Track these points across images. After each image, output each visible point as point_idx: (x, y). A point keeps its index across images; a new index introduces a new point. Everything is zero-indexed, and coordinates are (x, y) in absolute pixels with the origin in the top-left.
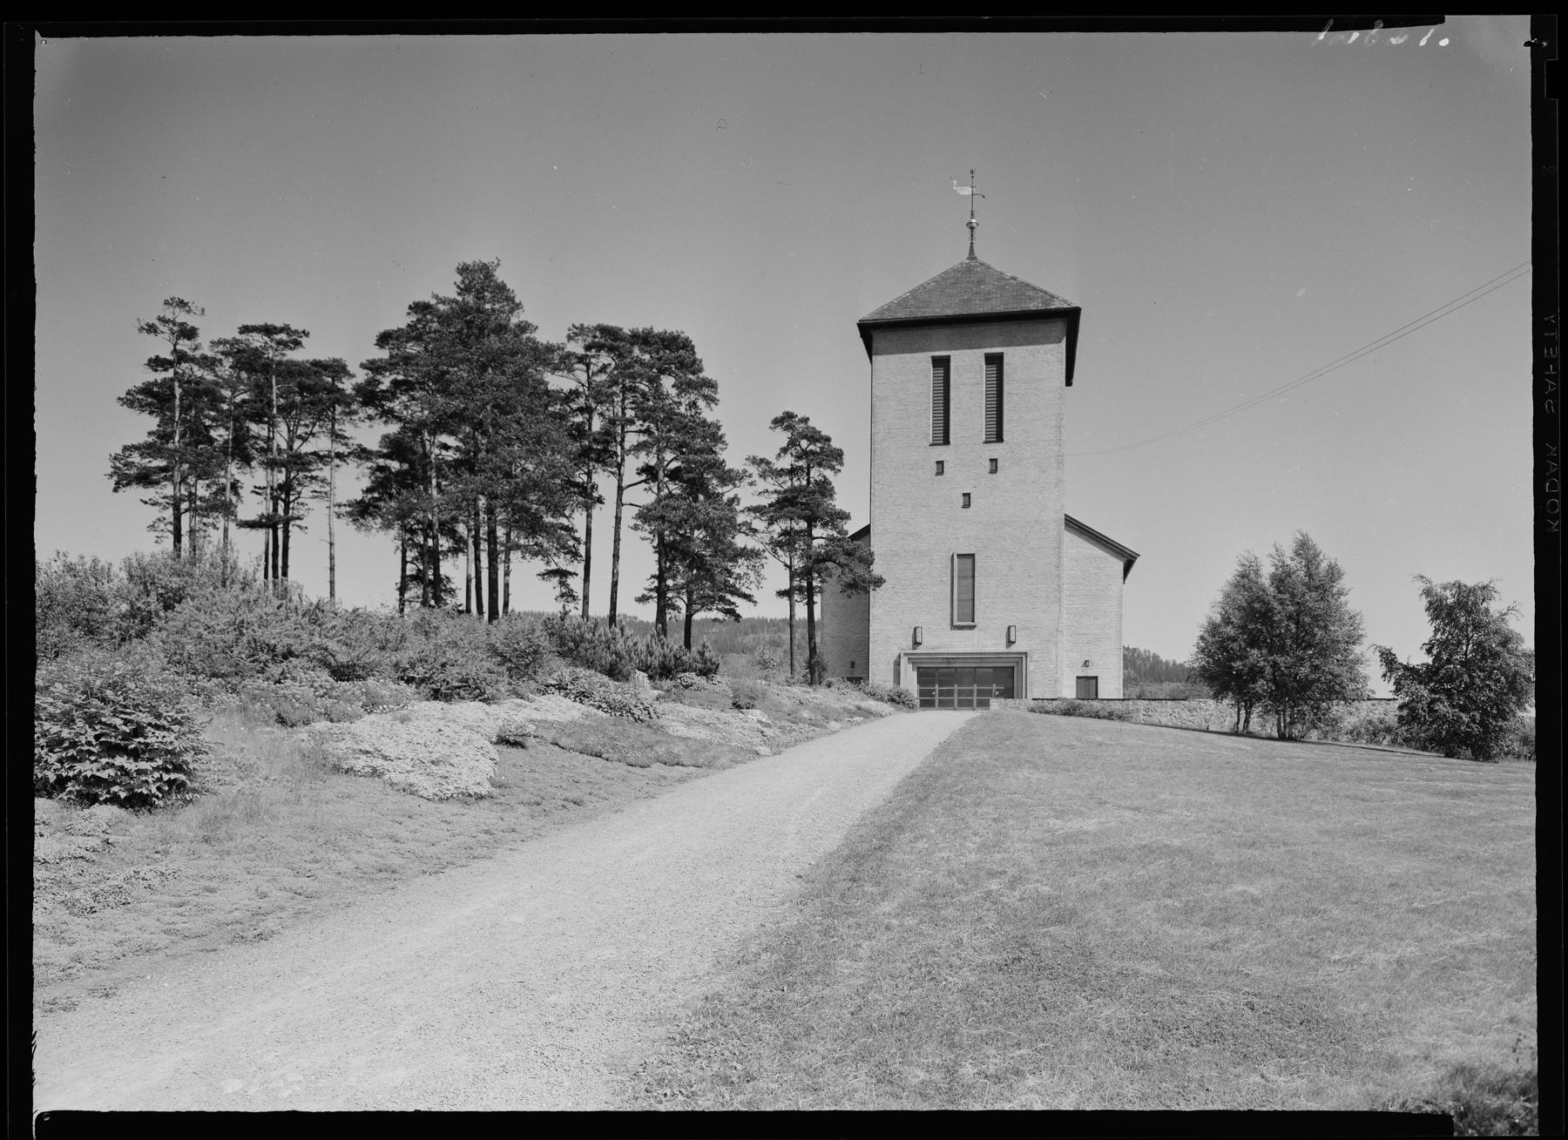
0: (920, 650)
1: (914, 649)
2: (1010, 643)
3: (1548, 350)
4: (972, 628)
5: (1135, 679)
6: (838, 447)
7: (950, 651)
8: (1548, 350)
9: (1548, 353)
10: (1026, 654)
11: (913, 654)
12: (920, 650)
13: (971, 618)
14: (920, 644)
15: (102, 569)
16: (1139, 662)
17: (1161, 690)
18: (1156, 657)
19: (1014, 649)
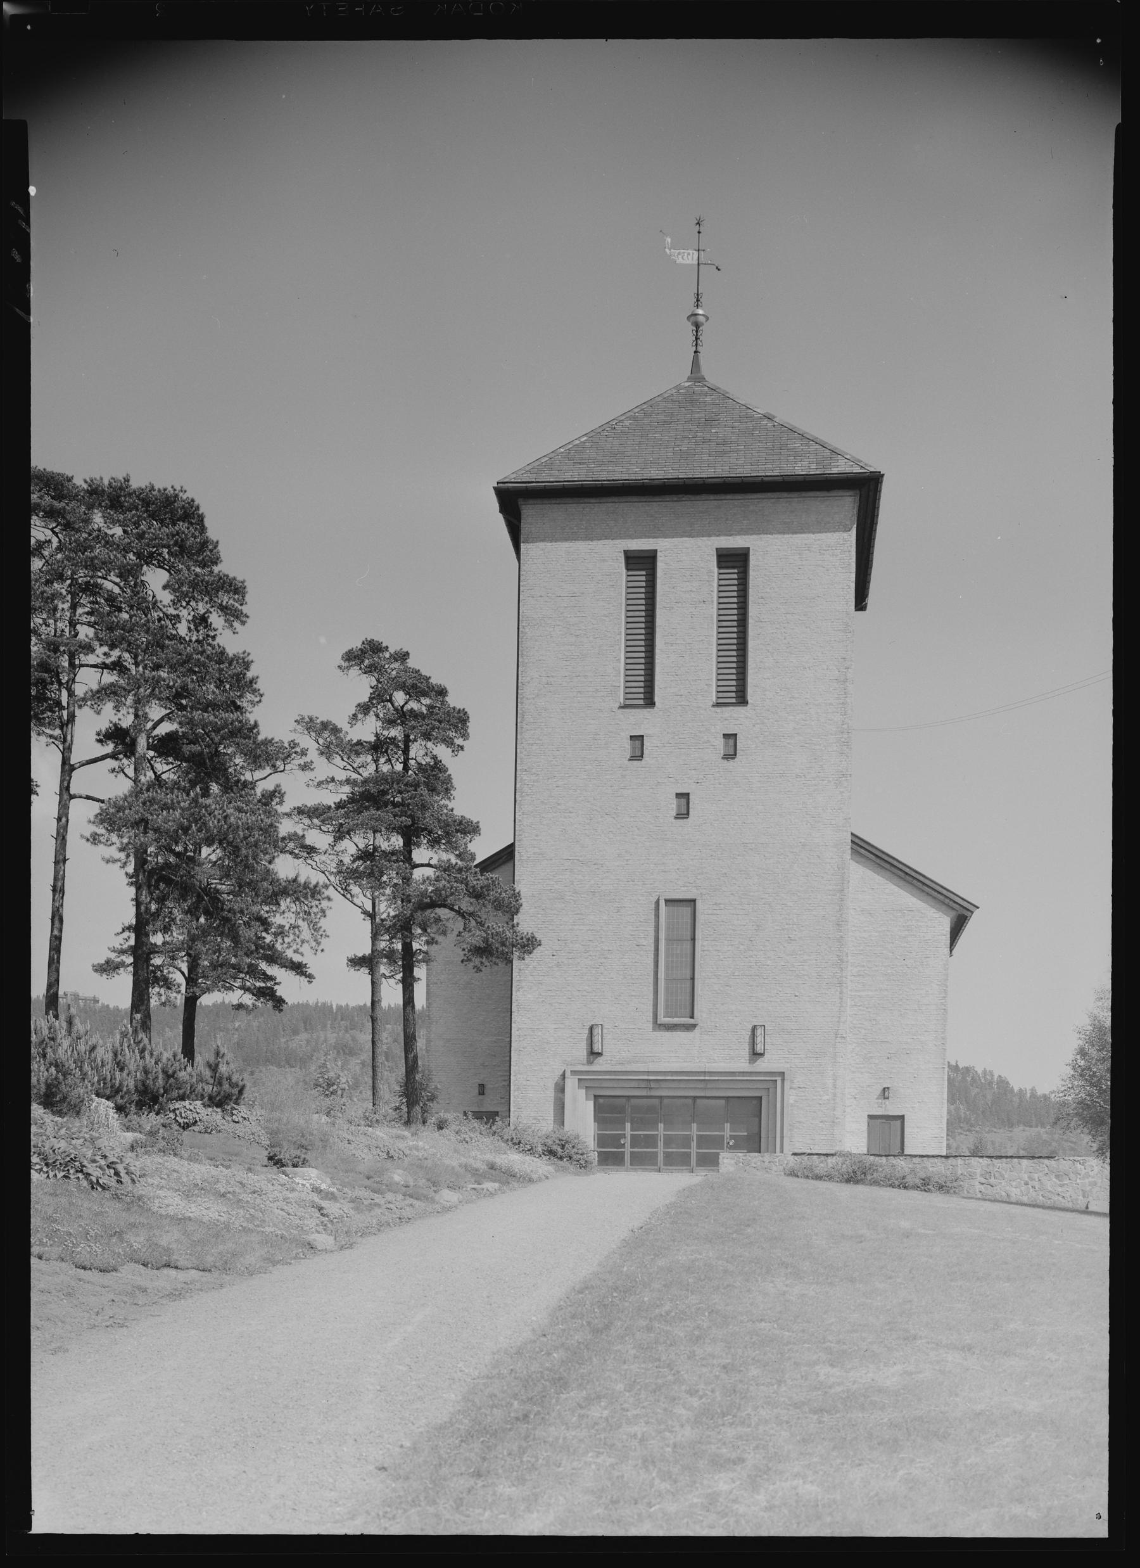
0: (600, 1065)
1: (590, 1063)
2: (755, 1055)
7: (652, 1067)
10: (782, 1074)
12: (600, 1065)
16: (974, 1091)
17: (1010, 1139)
19: (762, 1065)
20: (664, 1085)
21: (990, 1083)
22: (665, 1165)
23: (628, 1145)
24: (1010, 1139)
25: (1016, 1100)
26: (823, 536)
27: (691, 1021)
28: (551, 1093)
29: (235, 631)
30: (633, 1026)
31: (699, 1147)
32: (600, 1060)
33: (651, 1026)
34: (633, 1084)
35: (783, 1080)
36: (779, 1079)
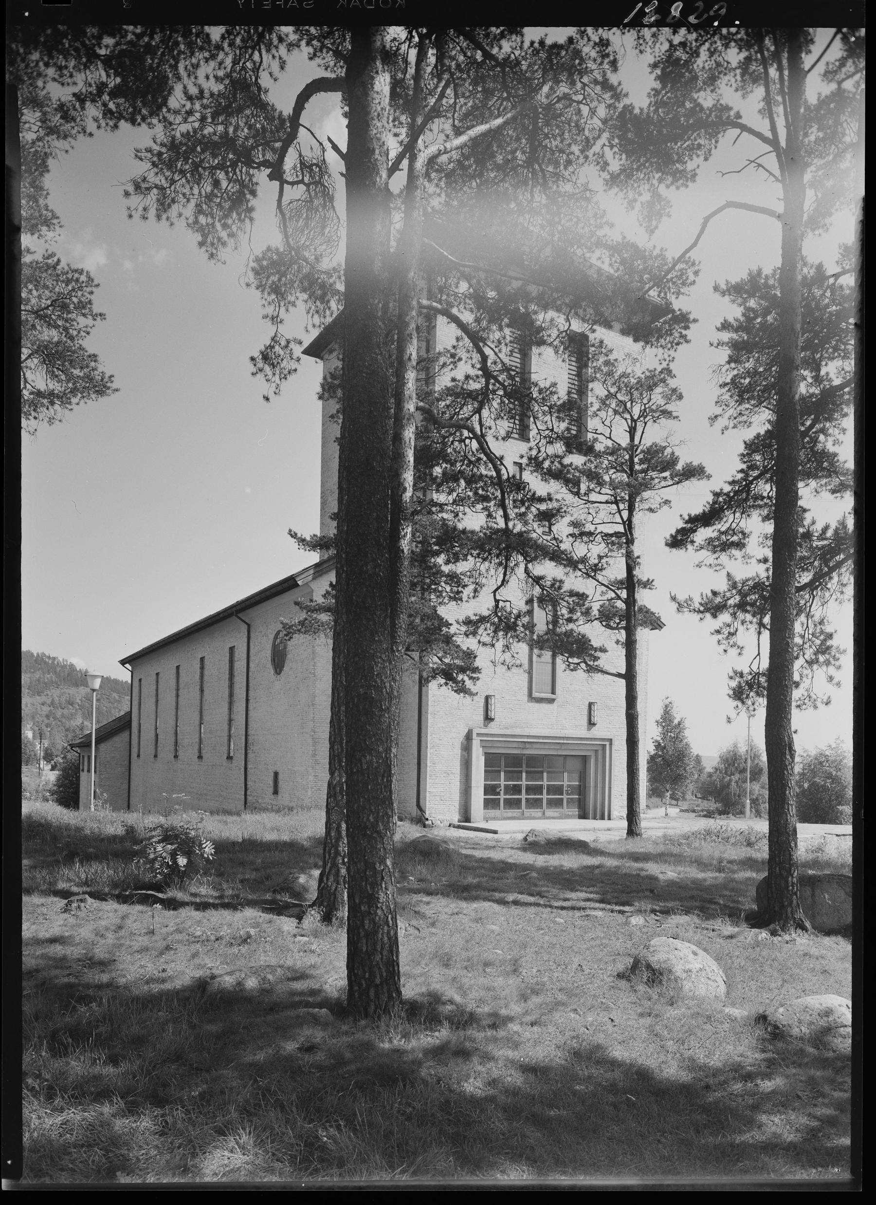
0: (493, 728)
1: (486, 726)
2: (591, 724)
3: (265, 5)
4: (551, 701)
5: (56, 683)
6: (566, 39)
7: (526, 732)
8: (265, 5)
9: (268, 5)
10: (610, 740)
11: (487, 735)
12: (493, 728)
13: (549, 688)
14: (493, 719)
15: (596, 659)
16: (58, 669)
17: (77, 692)
18: (72, 665)
19: (596, 732)
20: (535, 746)
21: (65, 666)
22: (526, 808)
23: (502, 793)
24: (77, 692)
25: (79, 675)
26: (337, 460)
27: (553, 696)
28: (458, 751)
29: (719, 404)
30: (514, 698)
31: (548, 794)
32: (492, 724)
33: (526, 698)
34: (514, 745)
35: (611, 744)
36: (607, 743)
